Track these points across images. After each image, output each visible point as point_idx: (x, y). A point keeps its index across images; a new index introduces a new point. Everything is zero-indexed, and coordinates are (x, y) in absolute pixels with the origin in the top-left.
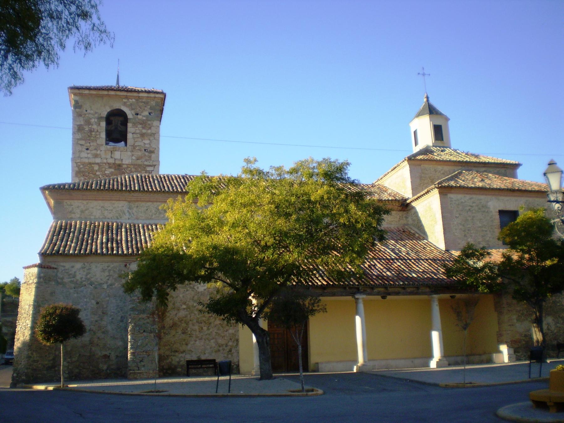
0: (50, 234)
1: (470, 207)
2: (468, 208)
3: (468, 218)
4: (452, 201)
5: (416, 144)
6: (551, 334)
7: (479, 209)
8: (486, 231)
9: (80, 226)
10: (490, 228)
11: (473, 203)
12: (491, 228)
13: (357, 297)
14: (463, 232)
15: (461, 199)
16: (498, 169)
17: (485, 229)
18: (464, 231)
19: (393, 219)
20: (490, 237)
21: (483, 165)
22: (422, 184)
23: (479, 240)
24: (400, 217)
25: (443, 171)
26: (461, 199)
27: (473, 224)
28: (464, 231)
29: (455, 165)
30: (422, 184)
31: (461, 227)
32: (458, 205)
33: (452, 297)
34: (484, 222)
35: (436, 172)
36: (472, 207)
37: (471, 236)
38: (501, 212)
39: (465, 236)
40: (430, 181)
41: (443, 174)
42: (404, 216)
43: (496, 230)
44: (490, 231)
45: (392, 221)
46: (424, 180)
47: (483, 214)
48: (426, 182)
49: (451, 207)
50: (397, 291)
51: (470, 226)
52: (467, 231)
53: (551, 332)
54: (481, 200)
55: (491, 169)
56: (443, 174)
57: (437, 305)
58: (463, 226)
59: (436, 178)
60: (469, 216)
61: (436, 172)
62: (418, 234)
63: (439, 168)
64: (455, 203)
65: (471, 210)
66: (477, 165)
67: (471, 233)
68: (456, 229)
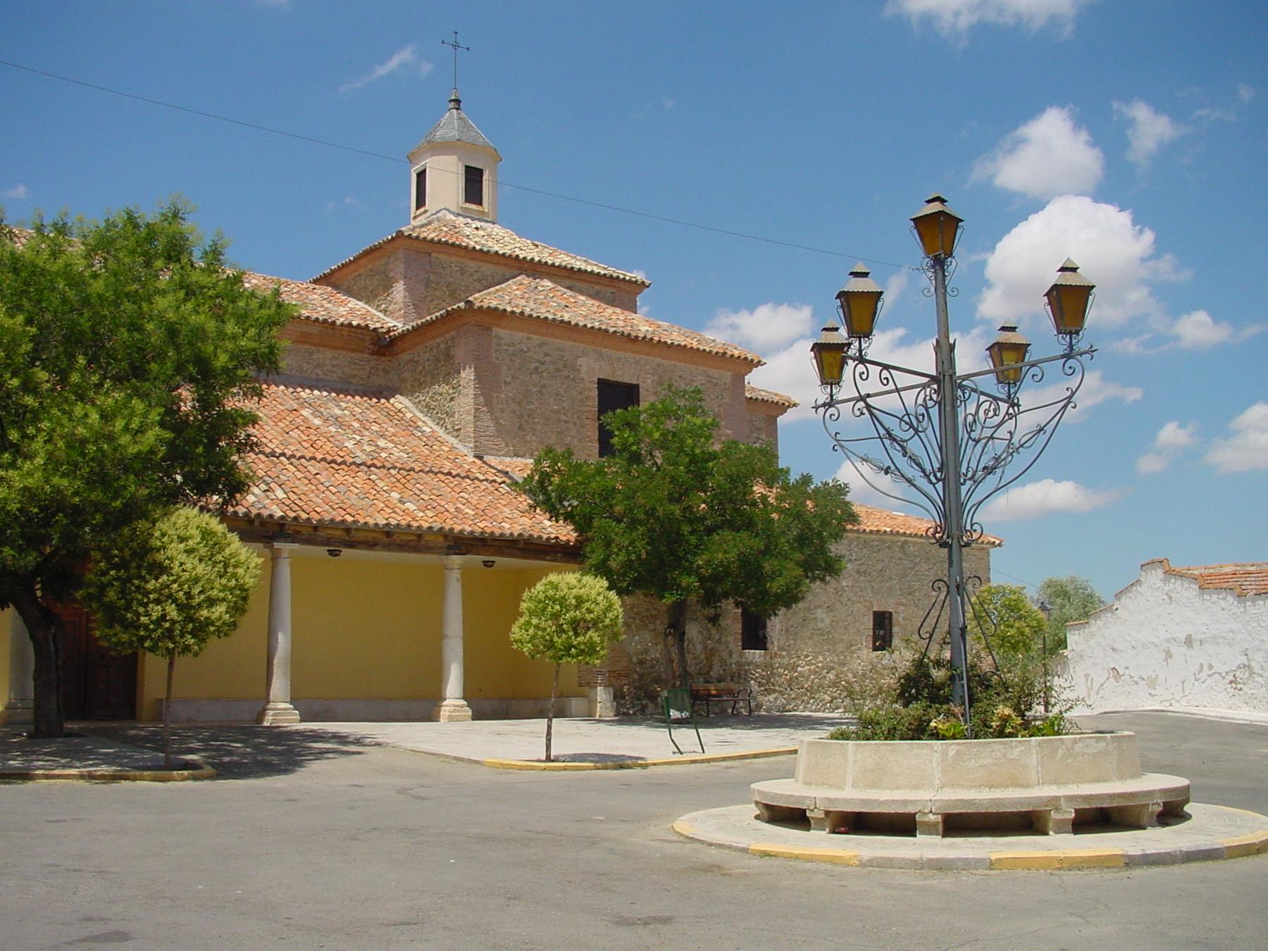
0: (1188, 715)
1: (537, 364)
2: (532, 366)
3: (530, 388)
4: (499, 344)
5: (421, 202)
6: (693, 661)
7: (557, 370)
8: (566, 422)
9: (431, 544)
10: (575, 417)
11: (546, 355)
12: (578, 417)
13: (277, 545)
14: (517, 420)
15: (521, 342)
16: (597, 287)
17: (566, 419)
18: (521, 417)
19: (355, 372)
20: (573, 437)
21: (567, 275)
22: (429, 299)
23: (549, 442)
24: (371, 368)
25: (479, 274)
26: (521, 342)
27: (541, 404)
28: (521, 417)
29: (506, 265)
30: (429, 299)
31: (513, 406)
32: (512, 354)
33: (487, 564)
34: (563, 401)
35: (462, 274)
36: (543, 363)
37: (534, 430)
38: (603, 384)
39: (520, 427)
40: (447, 293)
41: (479, 281)
42: (381, 367)
43: (588, 422)
44: (575, 424)
45: (354, 376)
46: (435, 289)
47: (563, 384)
48: (438, 293)
49: (497, 358)
50: (370, 538)
51: (533, 407)
52: (526, 417)
53: (694, 658)
54: (562, 350)
55: (583, 286)
56: (479, 281)
57: (458, 580)
58: (519, 404)
59: (463, 288)
60: (535, 385)
61: (462, 274)
62: (411, 412)
63: (472, 265)
64: (506, 350)
65: (540, 370)
66: (554, 272)
67: (534, 423)
68: (502, 411)
